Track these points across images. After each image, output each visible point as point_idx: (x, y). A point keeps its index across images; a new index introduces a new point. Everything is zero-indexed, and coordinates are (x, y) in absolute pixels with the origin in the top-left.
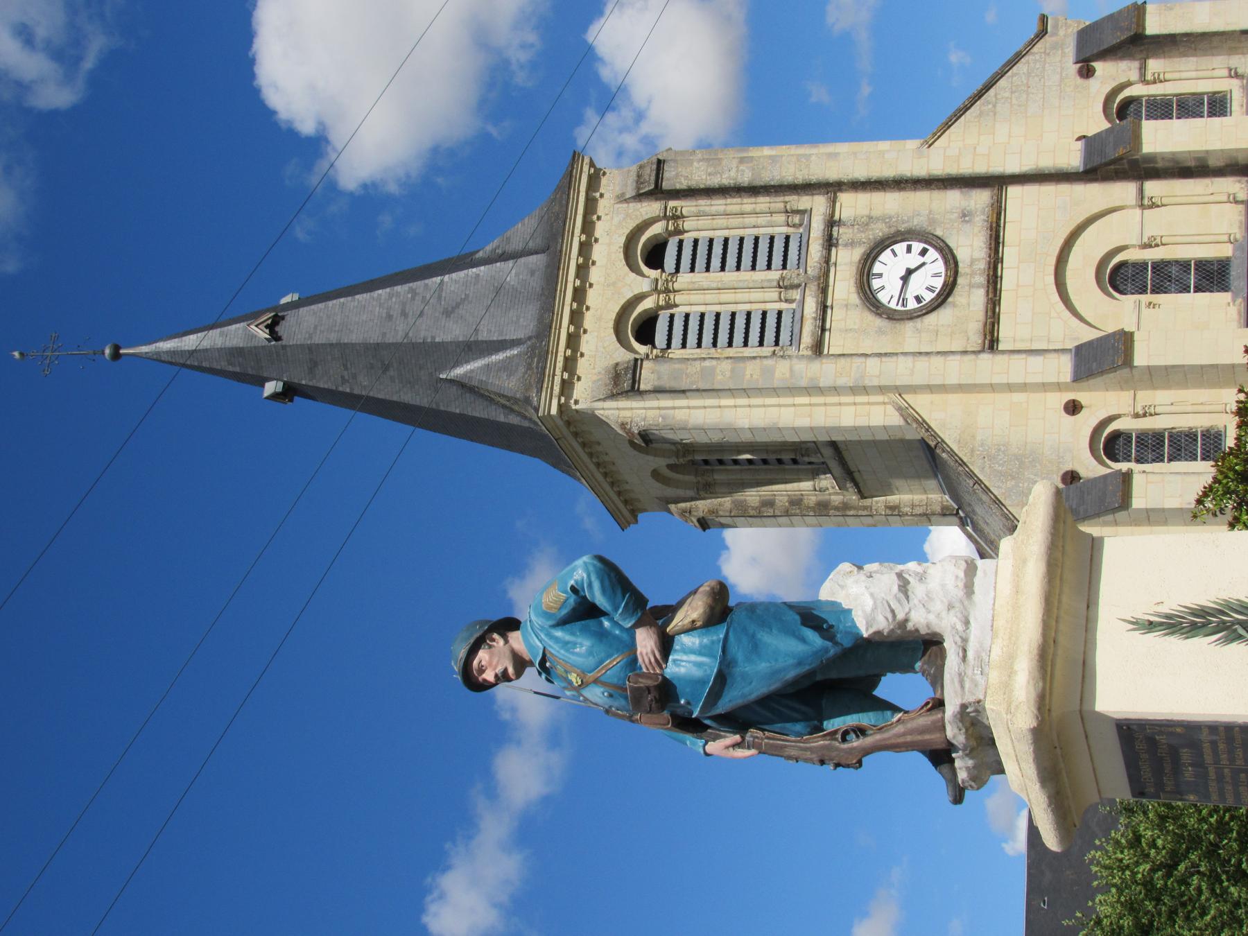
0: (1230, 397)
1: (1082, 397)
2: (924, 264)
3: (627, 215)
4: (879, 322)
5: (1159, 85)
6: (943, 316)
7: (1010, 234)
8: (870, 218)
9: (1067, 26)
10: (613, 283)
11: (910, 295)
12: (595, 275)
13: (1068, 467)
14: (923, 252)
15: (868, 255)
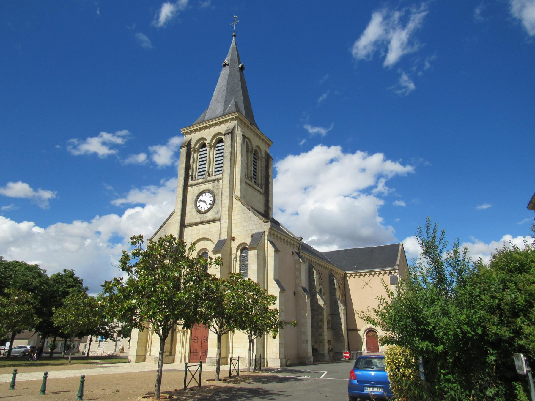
0: (254, 279)
12: (207, 130)
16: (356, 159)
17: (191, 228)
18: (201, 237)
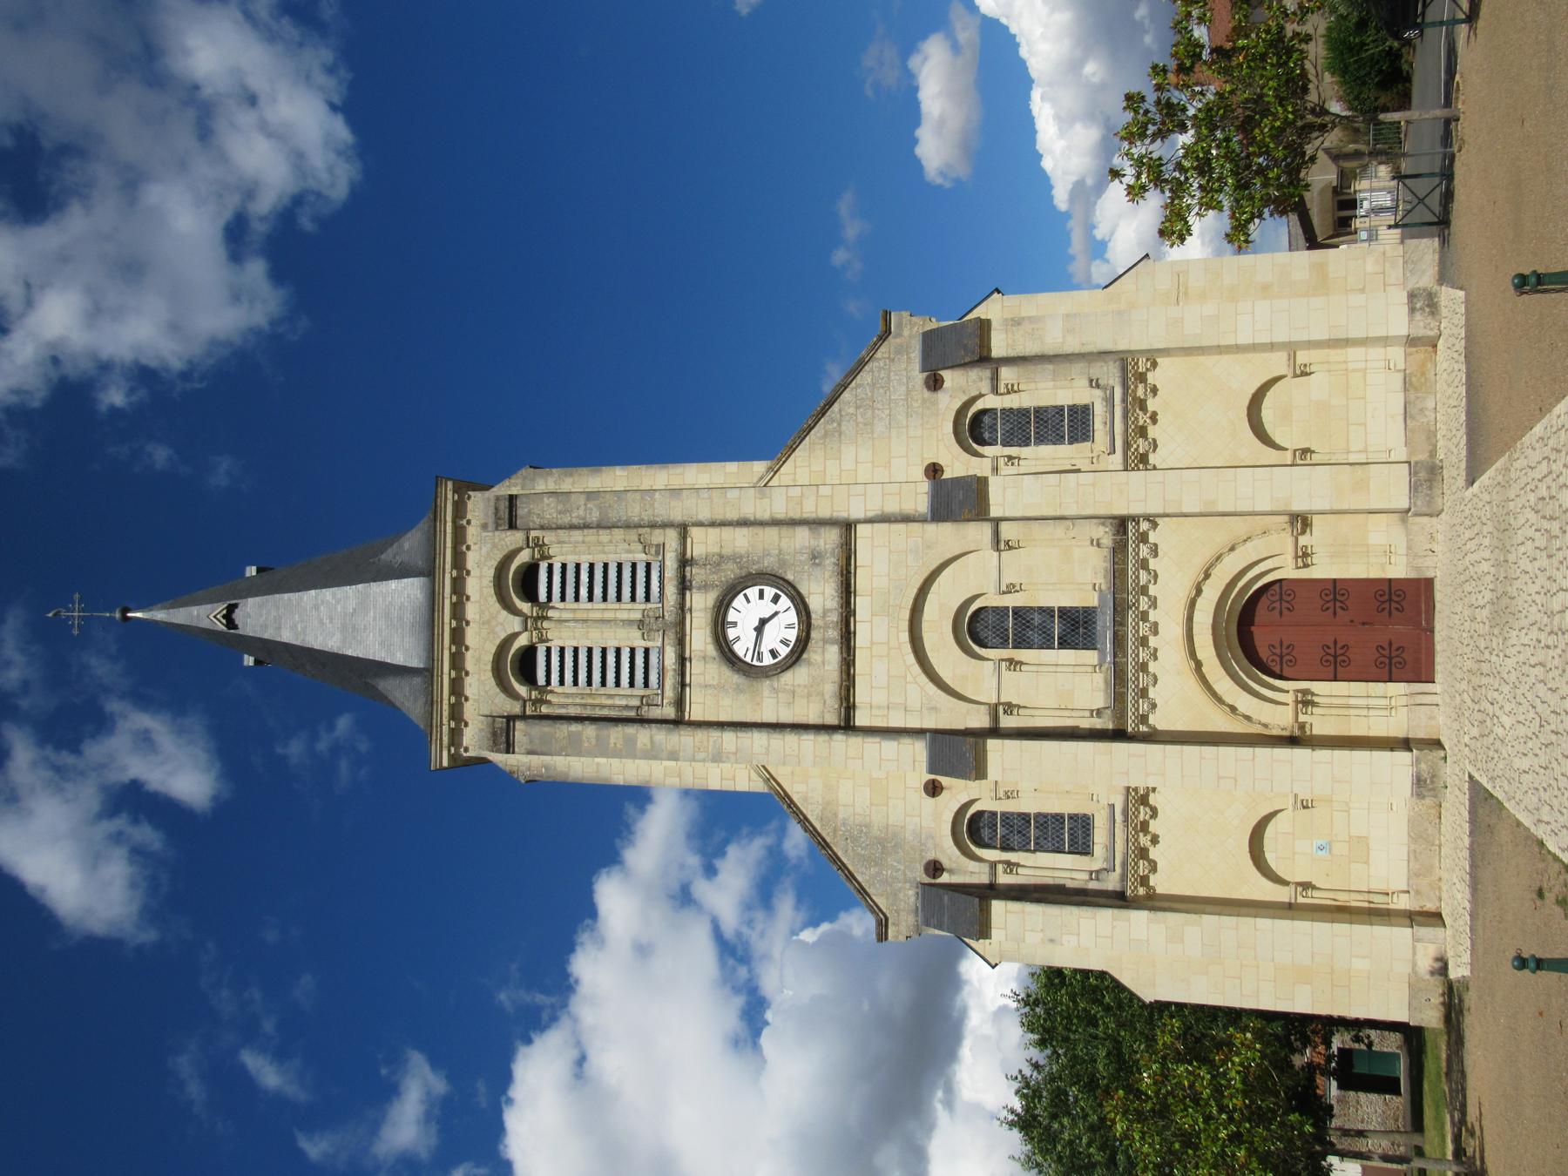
1: (944, 780)
2: (776, 613)
3: (494, 546)
4: (736, 679)
5: (1013, 396)
6: (798, 677)
7: (862, 581)
8: (721, 556)
9: (912, 325)
10: (489, 624)
11: (765, 649)
12: (471, 611)
13: (931, 856)
14: (776, 599)
15: (721, 602)
16: (593, 969)
17: (861, 695)
18: (905, 636)
